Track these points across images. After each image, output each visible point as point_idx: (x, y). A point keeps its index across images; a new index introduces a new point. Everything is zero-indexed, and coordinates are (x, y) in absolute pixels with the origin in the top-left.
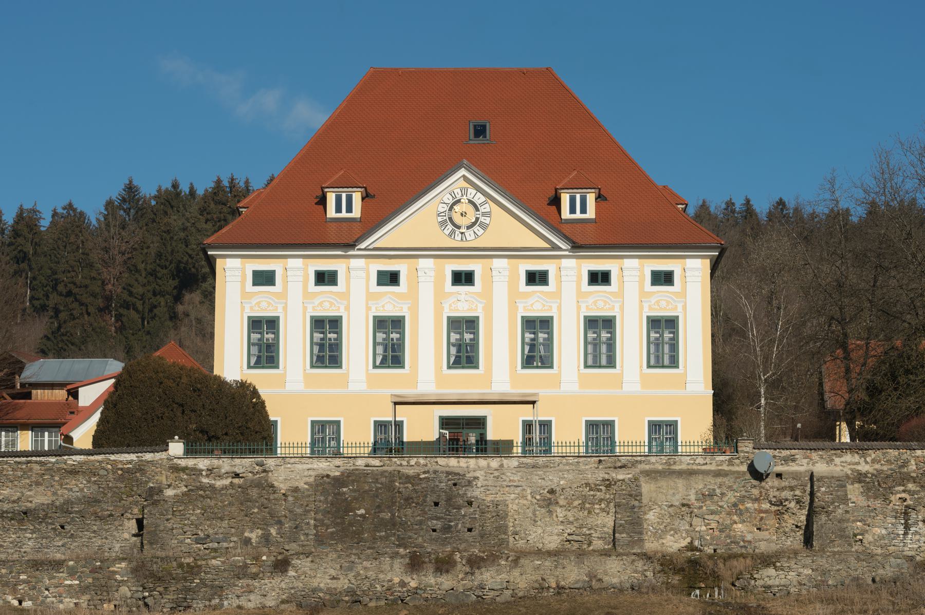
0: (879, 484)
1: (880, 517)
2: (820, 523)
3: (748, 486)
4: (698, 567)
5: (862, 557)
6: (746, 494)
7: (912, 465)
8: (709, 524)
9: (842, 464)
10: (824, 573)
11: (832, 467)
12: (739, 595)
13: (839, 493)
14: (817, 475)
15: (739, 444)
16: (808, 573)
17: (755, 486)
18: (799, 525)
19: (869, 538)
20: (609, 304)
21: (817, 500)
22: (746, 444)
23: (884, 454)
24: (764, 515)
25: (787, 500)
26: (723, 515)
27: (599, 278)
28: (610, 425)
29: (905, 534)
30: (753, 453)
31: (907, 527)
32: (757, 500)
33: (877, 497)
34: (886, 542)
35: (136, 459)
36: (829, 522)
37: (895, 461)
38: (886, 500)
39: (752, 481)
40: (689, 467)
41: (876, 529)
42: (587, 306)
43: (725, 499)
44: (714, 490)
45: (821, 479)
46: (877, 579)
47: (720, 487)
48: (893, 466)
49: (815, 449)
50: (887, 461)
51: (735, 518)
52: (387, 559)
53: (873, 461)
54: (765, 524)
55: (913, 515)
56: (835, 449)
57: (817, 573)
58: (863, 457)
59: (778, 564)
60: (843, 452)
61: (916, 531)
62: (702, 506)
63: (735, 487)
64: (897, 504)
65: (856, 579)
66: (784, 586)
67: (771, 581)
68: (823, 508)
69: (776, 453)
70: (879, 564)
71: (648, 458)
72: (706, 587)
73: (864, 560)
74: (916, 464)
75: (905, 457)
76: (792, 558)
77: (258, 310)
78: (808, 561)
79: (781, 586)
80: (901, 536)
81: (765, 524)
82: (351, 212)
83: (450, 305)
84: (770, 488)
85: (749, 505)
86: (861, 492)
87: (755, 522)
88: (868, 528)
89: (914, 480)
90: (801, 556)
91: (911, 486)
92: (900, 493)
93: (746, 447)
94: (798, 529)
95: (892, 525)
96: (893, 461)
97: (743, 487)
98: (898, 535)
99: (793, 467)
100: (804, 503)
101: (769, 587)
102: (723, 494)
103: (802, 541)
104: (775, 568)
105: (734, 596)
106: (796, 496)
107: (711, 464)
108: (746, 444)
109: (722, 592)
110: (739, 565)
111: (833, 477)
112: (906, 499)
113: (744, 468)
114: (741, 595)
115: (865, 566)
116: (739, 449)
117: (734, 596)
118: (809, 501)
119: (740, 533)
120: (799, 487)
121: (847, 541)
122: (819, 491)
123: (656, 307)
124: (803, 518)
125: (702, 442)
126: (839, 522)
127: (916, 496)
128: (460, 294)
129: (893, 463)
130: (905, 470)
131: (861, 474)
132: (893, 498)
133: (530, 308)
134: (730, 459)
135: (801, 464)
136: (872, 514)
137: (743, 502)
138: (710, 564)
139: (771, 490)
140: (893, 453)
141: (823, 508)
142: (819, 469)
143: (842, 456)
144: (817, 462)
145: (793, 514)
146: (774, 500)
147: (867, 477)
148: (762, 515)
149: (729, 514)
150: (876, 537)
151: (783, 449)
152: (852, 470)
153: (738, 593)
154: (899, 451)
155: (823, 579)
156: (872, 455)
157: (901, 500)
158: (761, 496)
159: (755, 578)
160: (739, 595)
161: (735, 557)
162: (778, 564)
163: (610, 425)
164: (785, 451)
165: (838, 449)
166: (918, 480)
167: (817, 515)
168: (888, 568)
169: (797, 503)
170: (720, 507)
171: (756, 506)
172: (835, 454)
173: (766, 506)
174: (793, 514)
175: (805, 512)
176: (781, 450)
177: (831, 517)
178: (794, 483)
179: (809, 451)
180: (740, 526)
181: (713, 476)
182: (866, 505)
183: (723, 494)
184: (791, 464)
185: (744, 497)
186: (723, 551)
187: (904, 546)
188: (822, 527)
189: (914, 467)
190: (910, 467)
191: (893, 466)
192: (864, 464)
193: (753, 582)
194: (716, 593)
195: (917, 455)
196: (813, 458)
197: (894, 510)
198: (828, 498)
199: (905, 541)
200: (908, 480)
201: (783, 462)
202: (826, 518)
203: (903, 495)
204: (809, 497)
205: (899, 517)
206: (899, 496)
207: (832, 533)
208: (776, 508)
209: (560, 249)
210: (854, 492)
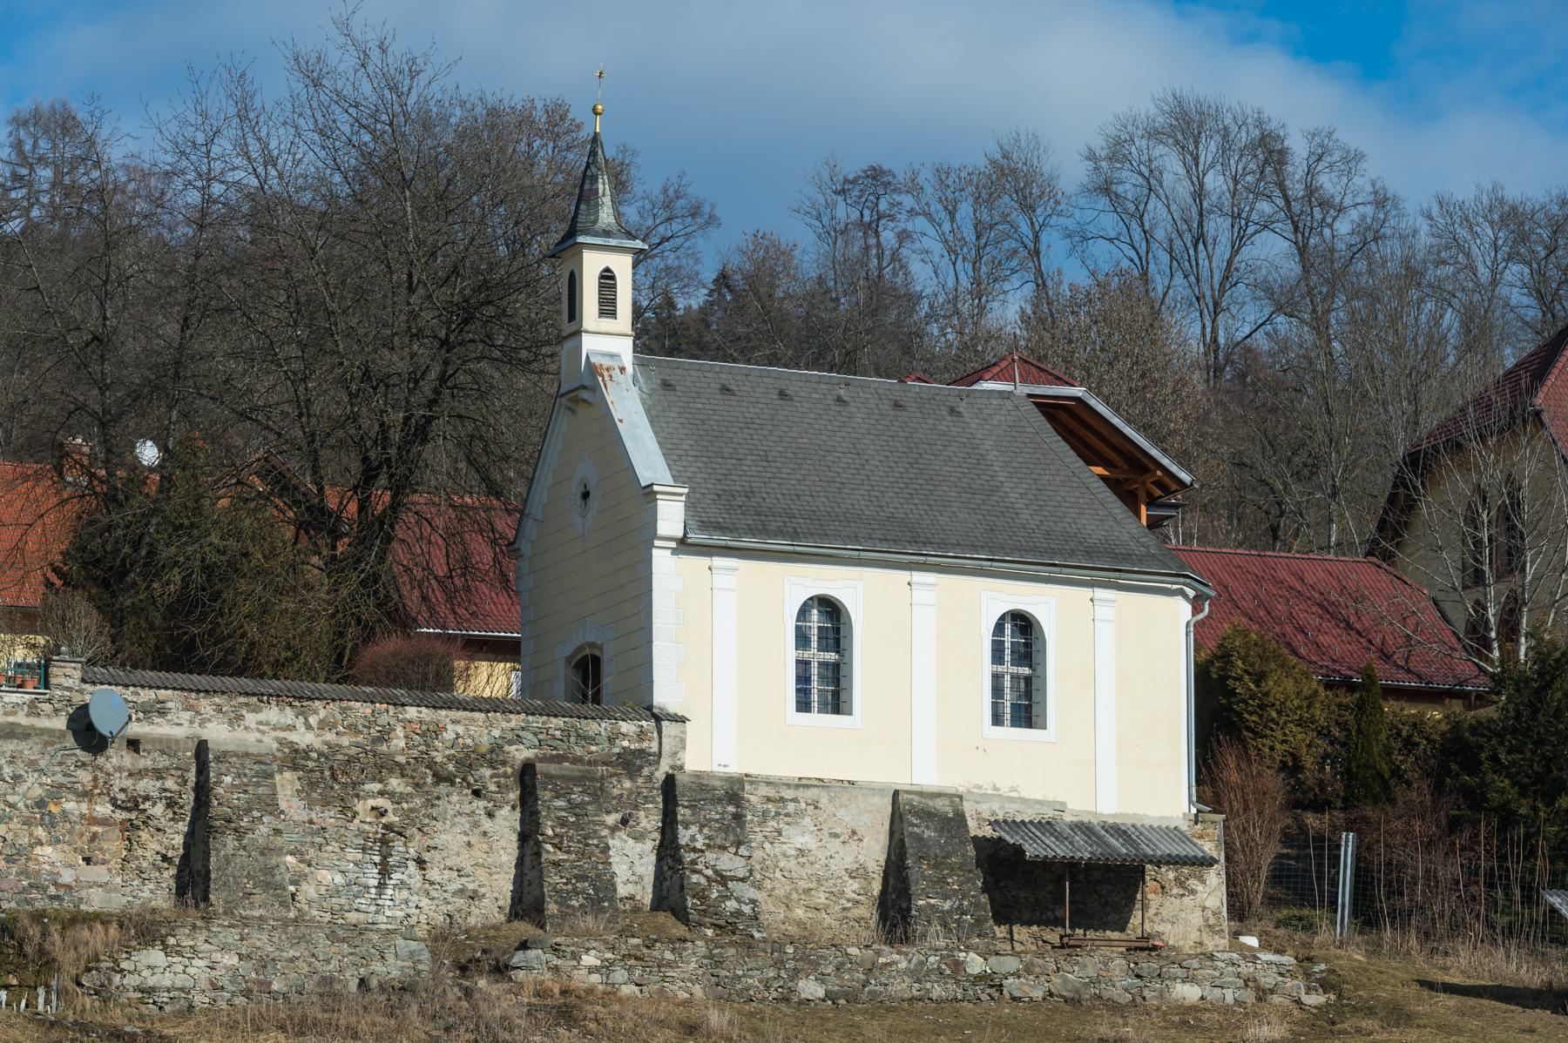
0: (334, 777)
1: (334, 846)
2: (223, 853)
3: (69, 762)
4: (6, 939)
5: (341, 933)
6: (65, 780)
7: (398, 738)
9: (261, 727)
10: (264, 964)
11: (239, 733)
12: (88, 1006)
13: (261, 790)
14: (216, 748)
15: (54, 670)
16: (231, 962)
17: (84, 764)
18: (170, 855)
19: (308, 891)
21: (216, 803)
22: (68, 671)
23: (343, 711)
24: (99, 829)
25: (147, 798)
26: (15, 824)
29: (381, 886)
30: (81, 692)
31: (385, 871)
32: (86, 795)
33: (328, 804)
34: (343, 901)
36: (242, 852)
37: (364, 726)
38: (348, 812)
39: (78, 752)
41: (324, 872)
43: (21, 789)
45: (222, 757)
46: (374, 983)
47: (11, 762)
48: (360, 739)
49: (207, 692)
50: (349, 727)
51: (40, 832)
53: (324, 725)
54: (101, 849)
55: (398, 845)
56: (247, 694)
57: (250, 965)
58: (302, 714)
59: (171, 941)
60: (262, 701)
61: (402, 882)
63: (43, 764)
64: (368, 820)
65: (328, 981)
66: (182, 989)
67: (155, 977)
68: (230, 821)
69: (128, 693)
70: (373, 951)
72: (20, 986)
73: (343, 940)
74: (406, 737)
75: (384, 719)
76: (200, 928)
78: (232, 936)
79: (176, 989)
80: (373, 891)
81: (101, 849)
84: (115, 771)
85: (70, 806)
86: (297, 791)
87: (79, 844)
88: (307, 870)
89: (402, 771)
90: (219, 925)
91: (395, 783)
92: (374, 797)
93: (67, 675)
94: (166, 865)
95: (356, 864)
96: (360, 728)
97: (60, 764)
98: (367, 887)
99: (160, 729)
100: (181, 807)
101: (151, 991)
102: (17, 778)
103: (174, 891)
104: (165, 947)
105: (79, 1008)
106: (165, 790)
108: (68, 671)
109: (54, 997)
110: (95, 938)
111: (247, 755)
112: (386, 811)
113: (60, 723)
114: (92, 1007)
115: (346, 952)
116: (53, 681)
117: (79, 1008)
118: (192, 803)
119: (47, 867)
120: (173, 772)
121: (278, 895)
122: (219, 782)
124: (179, 840)
126: (262, 854)
127: (405, 805)
129: (361, 732)
130: (384, 748)
131: (296, 751)
132: (360, 806)
134: (32, 702)
135: (177, 721)
136: (318, 840)
137: (56, 799)
138: (34, 931)
139: (117, 775)
140: (362, 709)
141: (230, 821)
142: (215, 735)
143: (261, 711)
144: (210, 720)
145: (159, 830)
146: (122, 796)
147: (308, 758)
148: (95, 829)
149: (27, 822)
150: (323, 890)
151: (142, 687)
152: (281, 742)
153: (88, 1000)
154: (372, 706)
155: (262, 977)
156: (321, 711)
157: (375, 812)
158: (95, 787)
159: (122, 970)
160: (88, 1006)
161: (84, 921)
162: (171, 941)
164: (146, 691)
165: (254, 694)
166: (409, 772)
167: (218, 835)
168: (391, 959)
169: (169, 806)
171: (84, 807)
172: (247, 705)
173: (103, 809)
174: (159, 830)
175: (183, 827)
176: (139, 690)
177: (245, 842)
178: (163, 762)
179: (193, 695)
180: (48, 850)
182: (306, 819)
184: (157, 720)
185: (61, 786)
186: (13, 905)
187: (377, 912)
188: (228, 862)
189: (402, 744)
190: (395, 741)
191: (360, 739)
192: (303, 729)
193: (117, 978)
194: (41, 1000)
195: (408, 716)
196: (203, 711)
197: (361, 833)
198: (238, 799)
199: (380, 902)
200: (391, 771)
201: (141, 715)
202: (236, 843)
203: (381, 802)
204: (192, 796)
205: (371, 849)
206: (371, 802)
207: (249, 876)
208: (125, 815)
210: (287, 784)
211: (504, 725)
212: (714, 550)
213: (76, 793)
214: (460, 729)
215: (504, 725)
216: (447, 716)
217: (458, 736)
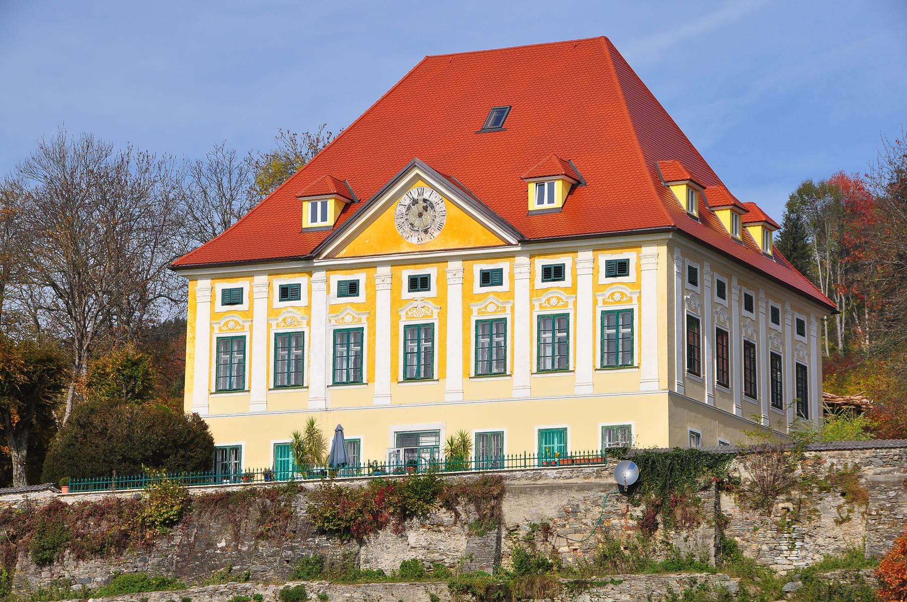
6: (612, 509)
8: (572, 544)
20: (563, 301)
27: (554, 273)
28: (499, 436)
35: (21, 498)
40: (555, 481)
42: (603, 299)
43: (589, 515)
44: (578, 506)
52: (207, 597)
62: (565, 524)
71: (514, 473)
77: (226, 330)
82: (553, 202)
83: (407, 313)
102: (587, 510)
107: (578, 476)
123: (547, 304)
125: (576, 453)
128: (416, 300)
133: (484, 310)
134: (598, 470)
148: (629, 532)
163: (499, 436)
170: (585, 524)
181: (577, 491)
183: (587, 510)
185: (610, 512)
190: (796, 471)
209: (510, 244)
211: (862, 455)
212: (704, 251)
213: (618, 515)
214: (835, 461)
215: (862, 455)
216: (827, 455)
217: (833, 464)
